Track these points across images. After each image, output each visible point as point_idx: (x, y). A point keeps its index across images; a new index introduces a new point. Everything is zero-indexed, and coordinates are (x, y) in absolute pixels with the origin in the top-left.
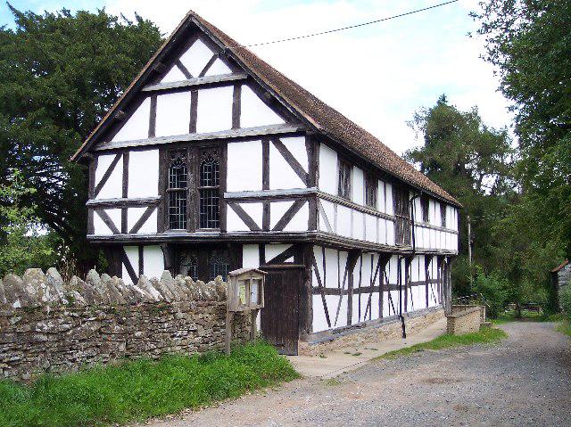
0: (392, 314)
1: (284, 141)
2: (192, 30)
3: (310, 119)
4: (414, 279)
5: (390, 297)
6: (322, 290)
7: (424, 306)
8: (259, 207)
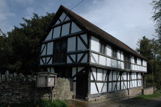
0: (125, 88)
1: (81, 36)
2: (62, 10)
3: (87, 28)
4: (133, 78)
5: (124, 84)
6: (94, 81)
7: (136, 86)
8: (75, 55)
